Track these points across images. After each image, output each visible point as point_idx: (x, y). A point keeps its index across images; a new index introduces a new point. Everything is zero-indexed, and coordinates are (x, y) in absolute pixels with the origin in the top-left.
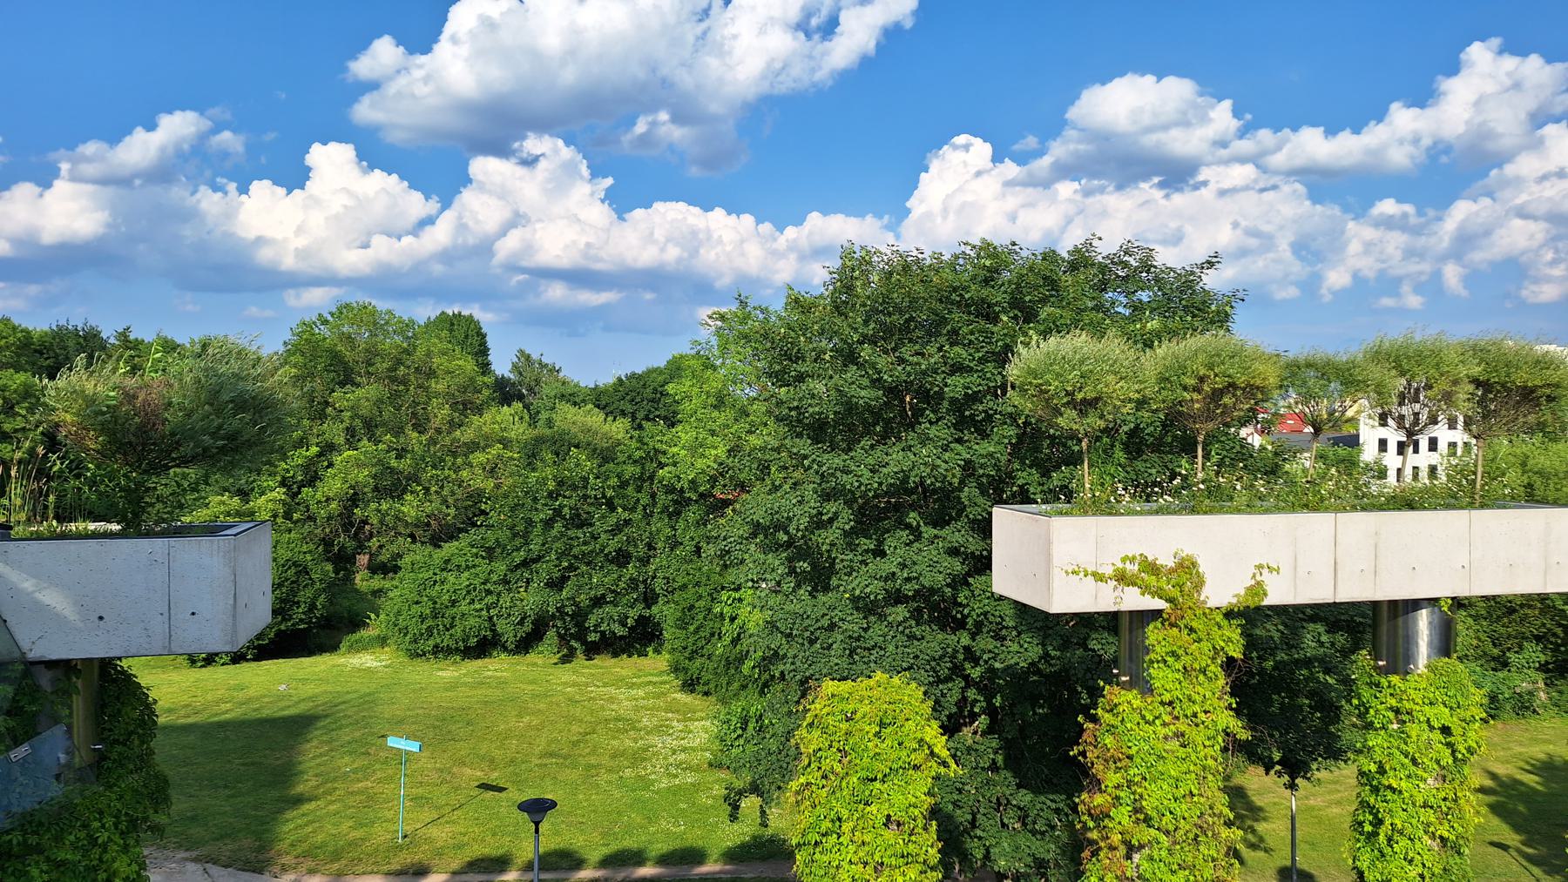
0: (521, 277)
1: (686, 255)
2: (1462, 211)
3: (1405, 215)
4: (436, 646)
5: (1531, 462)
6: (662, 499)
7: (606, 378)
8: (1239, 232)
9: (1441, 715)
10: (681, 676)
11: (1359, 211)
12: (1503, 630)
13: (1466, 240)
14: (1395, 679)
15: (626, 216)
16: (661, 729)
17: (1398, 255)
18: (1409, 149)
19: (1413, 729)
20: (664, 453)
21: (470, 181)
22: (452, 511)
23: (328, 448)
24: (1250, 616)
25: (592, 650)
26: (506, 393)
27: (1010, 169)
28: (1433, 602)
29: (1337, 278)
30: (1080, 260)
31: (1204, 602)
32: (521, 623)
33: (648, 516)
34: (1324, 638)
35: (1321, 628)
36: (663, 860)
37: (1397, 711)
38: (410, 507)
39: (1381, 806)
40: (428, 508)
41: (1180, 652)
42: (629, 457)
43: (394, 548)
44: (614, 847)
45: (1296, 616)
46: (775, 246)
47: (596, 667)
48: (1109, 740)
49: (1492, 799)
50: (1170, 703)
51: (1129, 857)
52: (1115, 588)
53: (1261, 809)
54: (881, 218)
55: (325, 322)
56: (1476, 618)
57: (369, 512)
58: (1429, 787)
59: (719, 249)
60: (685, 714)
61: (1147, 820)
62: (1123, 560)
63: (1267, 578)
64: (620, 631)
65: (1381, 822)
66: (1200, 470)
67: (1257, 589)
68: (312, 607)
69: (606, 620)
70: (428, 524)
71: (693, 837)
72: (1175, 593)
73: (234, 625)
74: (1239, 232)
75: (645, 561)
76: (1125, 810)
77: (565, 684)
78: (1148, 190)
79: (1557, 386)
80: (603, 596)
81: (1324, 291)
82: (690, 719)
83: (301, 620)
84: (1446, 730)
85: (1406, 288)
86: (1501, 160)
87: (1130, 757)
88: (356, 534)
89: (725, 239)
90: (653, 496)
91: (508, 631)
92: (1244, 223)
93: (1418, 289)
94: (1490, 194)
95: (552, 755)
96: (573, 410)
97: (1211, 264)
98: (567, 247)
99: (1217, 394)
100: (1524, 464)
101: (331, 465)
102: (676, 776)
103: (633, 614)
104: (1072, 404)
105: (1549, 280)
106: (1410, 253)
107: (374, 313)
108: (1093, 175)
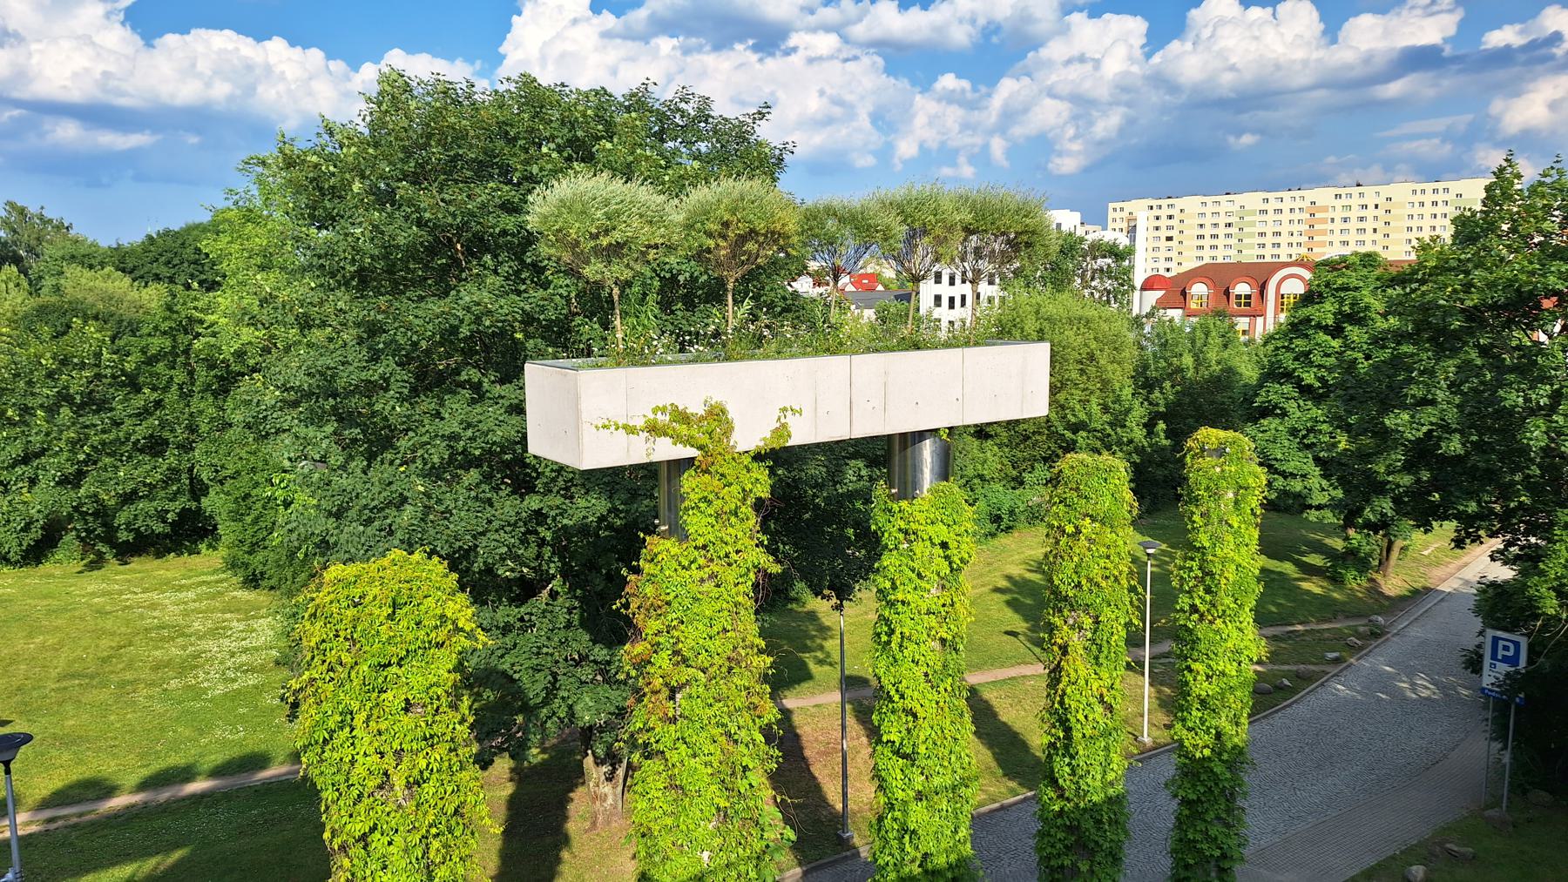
0: (16, 112)
1: (238, 92)
2: (1008, 88)
3: (963, 91)
5: (1043, 310)
6: (202, 375)
7: (132, 237)
8: (825, 100)
10: (241, 572)
11: (925, 85)
12: (1019, 455)
13: (1010, 116)
14: (904, 504)
15: (157, 42)
16: (216, 632)
17: (957, 128)
18: (967, 28)
19: (918, 548)
20: (201, 322)
21: (149, 45)
24: (779, 458)
25: (126, 552)
27: (608, 20)
28: (934, 432)
29: (906, 148)
30: (638, 102)
31: (734, 447)
32: (26, 529)
33: (186, 396)
34: (863, 473)
35: (861, 464)
36: (216, 773)
37: (906, 533)
39: (894, 617)
41: (711, 497)
42: (156, 328)
44: (156, 766)
45: (838, 452)
46: (349, 86)
47: (135, 571)
48: (649, 590)
49: (1008, 597)
50: (704, 547)
51: (672, 698)
52: (647, 440)
53: (829, 629)
54: (472, 63)
56: (1000, 446)
58: (932, 596)
59: (281, 87)
60: (247, 612)
61: (685, 660)
62: (655, 411)
63: (791, 420)
64: (159, 528)
65: (892, 632)
66: (734, 314)
67: (782, 430)
71: (253, 742)
72: (704, 440)
74: (825, 100)
75: (186, 447)
76: (665, 654)
77: (93, 594)
78: (742, 52)
79: (1033, 233)
80: (134, 492)
81: (896, 160)
82: (253, 617)
84: (944, 545)
85: (962, 159)
86: (1036, 44)
87: (668, 603)
89: (289, 75)
90: (191, 373)
92: (829, 91)
93: (972, 160)
94: (1029, 75)
95: (73, 676)
96: (88, 274)
97: (762, 115)
98: (75, 75)
99: (742, 239)
100: (1037, 312)
102: (234, 680)
103: (177, 506)
104: (597, 251)
105: (1069, 153)
106: (966, 126)
108: (689, 33)
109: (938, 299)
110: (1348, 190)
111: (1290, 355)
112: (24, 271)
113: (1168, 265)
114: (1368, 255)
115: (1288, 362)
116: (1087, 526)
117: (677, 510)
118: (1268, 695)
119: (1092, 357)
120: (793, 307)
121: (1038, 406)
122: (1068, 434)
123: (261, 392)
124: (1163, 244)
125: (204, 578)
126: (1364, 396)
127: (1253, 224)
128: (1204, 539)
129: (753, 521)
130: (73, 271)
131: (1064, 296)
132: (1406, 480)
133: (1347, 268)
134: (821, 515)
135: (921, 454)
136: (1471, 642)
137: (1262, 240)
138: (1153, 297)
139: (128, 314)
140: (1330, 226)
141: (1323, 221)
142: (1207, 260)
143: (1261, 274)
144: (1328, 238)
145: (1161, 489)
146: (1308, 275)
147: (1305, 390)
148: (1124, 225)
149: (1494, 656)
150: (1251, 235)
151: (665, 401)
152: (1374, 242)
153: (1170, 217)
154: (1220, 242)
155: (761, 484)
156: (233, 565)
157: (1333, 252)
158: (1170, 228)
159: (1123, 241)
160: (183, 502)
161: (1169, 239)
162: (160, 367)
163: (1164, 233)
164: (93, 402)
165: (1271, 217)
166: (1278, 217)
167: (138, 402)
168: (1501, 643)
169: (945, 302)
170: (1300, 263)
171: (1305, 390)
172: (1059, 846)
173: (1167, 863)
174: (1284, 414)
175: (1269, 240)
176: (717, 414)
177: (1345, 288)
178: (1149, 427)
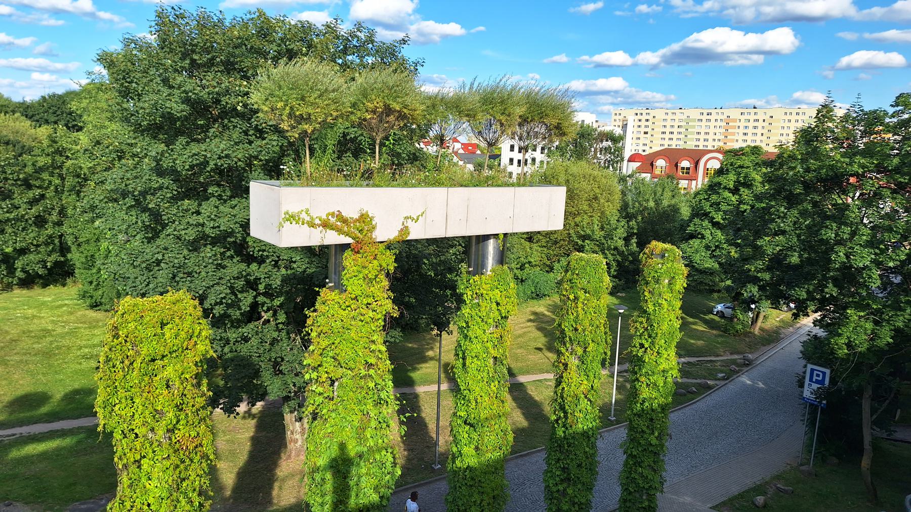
7: (31, 96)
9: (497, 295)
14: (477, 278)
28: (496, 236)
63: (410, 223)
67: (405, 230)
75: (59, 224)
109: (511, 160)
110: (749, 110)
111: (709, 204)
113: (644, 148)
114: (755, 147)
115: (707, 207)
116: (581, 294)
117: (340, 275)
118: (683, 394)
119: (596, 198)
120: (416, 158)
121: (556, 223)
122: (580, 242)
123: (93, 194)
124: (642, 135)
125: (66, 302)
126: (745, 227)
127: (694, 127)
128: (650, 308)
129: (386, 283)
131: (583, 163)
132: (767, 276)
133: (743, 154)
134: (426, 281)
135: (487, 248)
136: (800, 370)
137: (698, 137)
138: (635, 165)
139: (29, 143)
140: (737, 130)
141: (734, 127)
142: (666, 146)
143: (696, 156)
144: (735, 138)
145: (628, 277)
146: (720, 156)
147: (716, 225)
148: (621, 124)
149: (811, 380)
150: (692, 133)
151: (334, 209)
152: (761, 141)
153: (647, 120)
154: (675, 136)
155: (389, 261)
156: (84, 296)
157: (737, 146)
158: (647, 126)
159: (618, 131)
160: (55, 257)
161: (646, 133)
162: (45, 176)
163: (643, 130)
165: (704, 123)
166: (708, 124)
167: (30, 194)
168: (815, 372)
169: (515, 162)
170: (718, 151)
171: (716, 225)
172: (557, 479)
173: (618, 490)
174: (703, 237)
175: (702, 137)
176: (364, 218)
177: (741, 167)
178: (627, 240)
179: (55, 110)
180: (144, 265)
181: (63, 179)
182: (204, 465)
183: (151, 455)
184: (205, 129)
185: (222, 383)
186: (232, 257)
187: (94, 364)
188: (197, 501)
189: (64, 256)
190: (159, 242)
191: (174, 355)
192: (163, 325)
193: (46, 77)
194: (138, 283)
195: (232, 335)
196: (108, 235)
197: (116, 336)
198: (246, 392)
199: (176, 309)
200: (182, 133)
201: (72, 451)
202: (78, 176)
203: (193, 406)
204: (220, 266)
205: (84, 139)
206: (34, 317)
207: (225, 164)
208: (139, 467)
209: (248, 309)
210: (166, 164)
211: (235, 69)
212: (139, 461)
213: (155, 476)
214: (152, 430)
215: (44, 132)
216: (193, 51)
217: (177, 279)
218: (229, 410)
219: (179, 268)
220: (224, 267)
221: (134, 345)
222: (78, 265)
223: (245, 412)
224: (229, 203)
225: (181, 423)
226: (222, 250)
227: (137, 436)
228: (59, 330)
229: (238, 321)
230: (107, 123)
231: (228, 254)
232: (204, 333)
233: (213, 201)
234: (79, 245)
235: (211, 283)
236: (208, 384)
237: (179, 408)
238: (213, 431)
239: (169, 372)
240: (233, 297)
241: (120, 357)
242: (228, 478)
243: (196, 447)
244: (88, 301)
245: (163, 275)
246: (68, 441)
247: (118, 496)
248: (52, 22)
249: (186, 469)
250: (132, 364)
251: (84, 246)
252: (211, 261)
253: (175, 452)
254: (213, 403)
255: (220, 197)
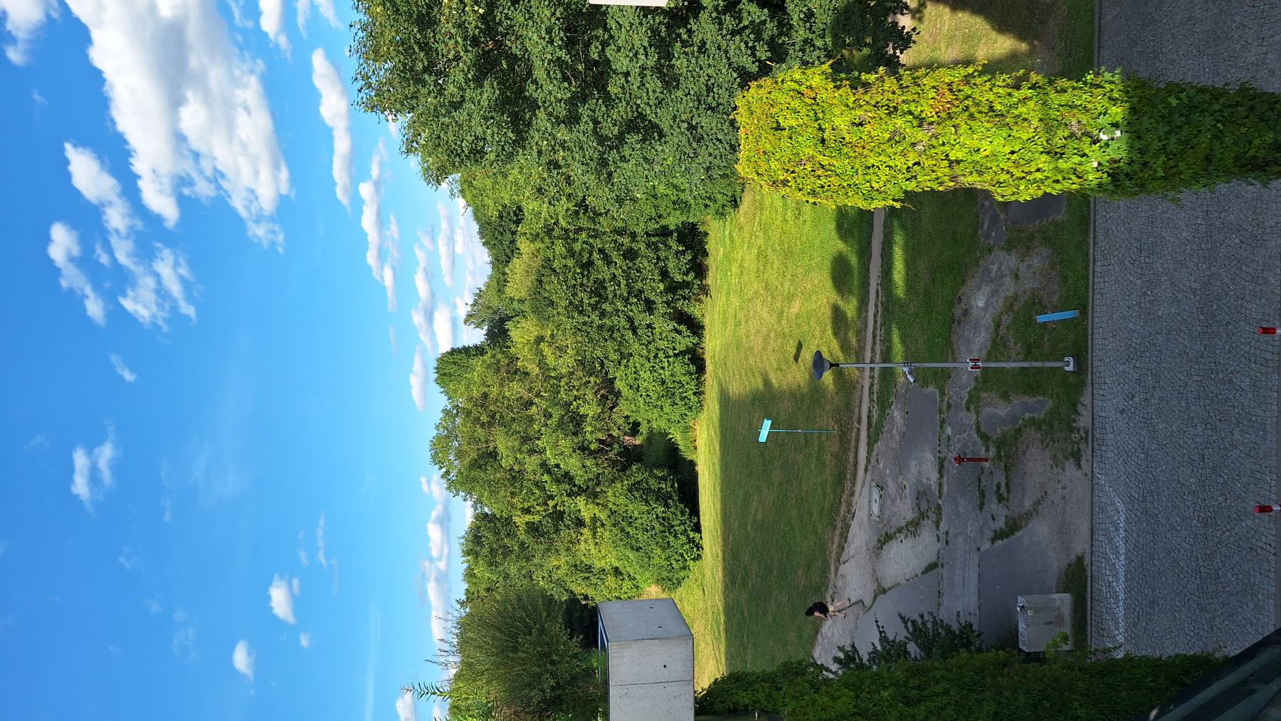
4: (695, 394)
22: (592, 379)
23: (544, 465)
26: (498, 333)
38: (590, 409)
40: (590, 396)
43: (620, 421)
55: (447, 473)
57: (591, 434)
68: (663, 479)
69: (677, 268)
70: (602, 396)
73: (673, 638)
75: (633, 236)
83: (672, 486)
88: (608, 446)
91: (684, 342)
101: (557, 466)
107: (438, 438)
112: (510, 318)
123: (600, 197)
130: (510, 291)
139: (537, 263)
156: (721, 214)
160: (672, 242)
162: (577, 247)
164: (599, 291)
167: (599, 263)
179: (500, 231)
180: (695, 145)
181: (581, 229)
182: (978, 81)
183: (947, 148)
184: (513, 59)
185: (866, 51)
186: (690, 32)
187: (807, 208)
188: (1025, 92)
189: (671, 233)
190: (665, 127)
191: (821, 115)
192: (779, 128)
193: (459, 238)
194: (717, 152)
195: (800, 34)
196: (651, 182)
197: (785, 183)
198: (886, 16)
199: (758, 111)
200: (522, 90)
201: (911, 234)
202: (577, 213)
203: (894, 93)
204: (702, 47)
205: (530, 206)
206: (741, 266)
207: (559, 36)
208: (958, 162)
209: (766, 11)
210: (562, 111)
211: (428, 14)
212: (951, 162)
213: (976, 144)
214: (914, 145)
215: (524, 246)
216: (412, 69)
217: (714, 104)
218: (904, 41)
219: (699, 101)
220: (703, 43)
221: (800, 163)
222: (684, 218)
223: (913, 17)
224: (614, 32)
225: (913, 108)
226: (679, 44)
227: (917, 164)
228: (761, 242)
229: (781, 24)
230: (511, 178)
231: (685, 37)
232: (797, 76)
233: (609, 52)
234: (660, 217)
235: (725, 61)
236: (868, 72)
237: (892, 111)
238: (931, 66)
239: (841, 122)
240: (747, 32)
241: (813, 179)
242: (1003, 45)
243: (951, 90)
244: (729, 209)
245: (707, 122)
246: (899, 238)
247: (990, 188)
248: (394, 227)
249: (977, 105)
250: (823, 167)
251: (662, 211)
252: (693, 61)
253: (950, 118)
254: (893, 65)
255: (605, 44)
